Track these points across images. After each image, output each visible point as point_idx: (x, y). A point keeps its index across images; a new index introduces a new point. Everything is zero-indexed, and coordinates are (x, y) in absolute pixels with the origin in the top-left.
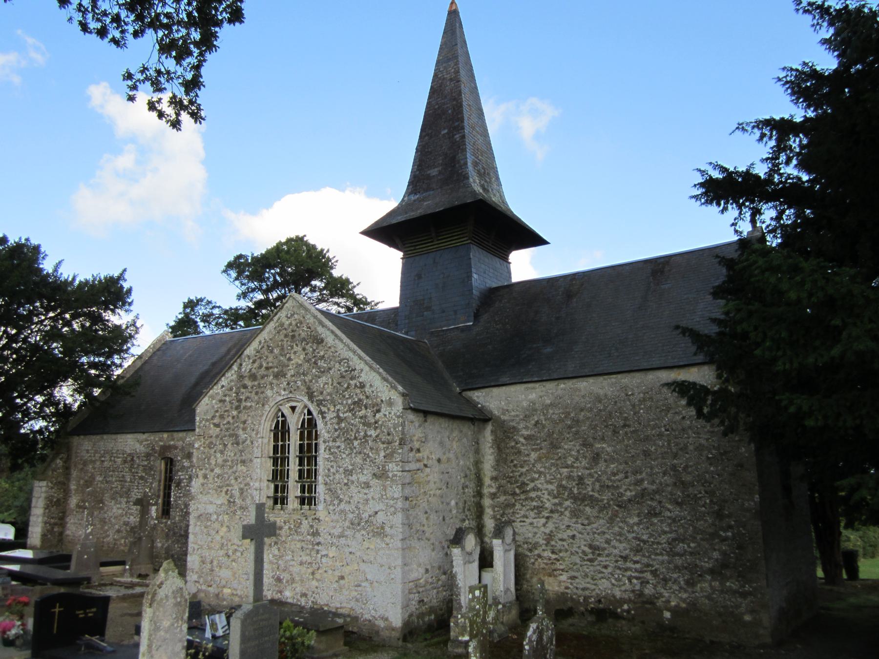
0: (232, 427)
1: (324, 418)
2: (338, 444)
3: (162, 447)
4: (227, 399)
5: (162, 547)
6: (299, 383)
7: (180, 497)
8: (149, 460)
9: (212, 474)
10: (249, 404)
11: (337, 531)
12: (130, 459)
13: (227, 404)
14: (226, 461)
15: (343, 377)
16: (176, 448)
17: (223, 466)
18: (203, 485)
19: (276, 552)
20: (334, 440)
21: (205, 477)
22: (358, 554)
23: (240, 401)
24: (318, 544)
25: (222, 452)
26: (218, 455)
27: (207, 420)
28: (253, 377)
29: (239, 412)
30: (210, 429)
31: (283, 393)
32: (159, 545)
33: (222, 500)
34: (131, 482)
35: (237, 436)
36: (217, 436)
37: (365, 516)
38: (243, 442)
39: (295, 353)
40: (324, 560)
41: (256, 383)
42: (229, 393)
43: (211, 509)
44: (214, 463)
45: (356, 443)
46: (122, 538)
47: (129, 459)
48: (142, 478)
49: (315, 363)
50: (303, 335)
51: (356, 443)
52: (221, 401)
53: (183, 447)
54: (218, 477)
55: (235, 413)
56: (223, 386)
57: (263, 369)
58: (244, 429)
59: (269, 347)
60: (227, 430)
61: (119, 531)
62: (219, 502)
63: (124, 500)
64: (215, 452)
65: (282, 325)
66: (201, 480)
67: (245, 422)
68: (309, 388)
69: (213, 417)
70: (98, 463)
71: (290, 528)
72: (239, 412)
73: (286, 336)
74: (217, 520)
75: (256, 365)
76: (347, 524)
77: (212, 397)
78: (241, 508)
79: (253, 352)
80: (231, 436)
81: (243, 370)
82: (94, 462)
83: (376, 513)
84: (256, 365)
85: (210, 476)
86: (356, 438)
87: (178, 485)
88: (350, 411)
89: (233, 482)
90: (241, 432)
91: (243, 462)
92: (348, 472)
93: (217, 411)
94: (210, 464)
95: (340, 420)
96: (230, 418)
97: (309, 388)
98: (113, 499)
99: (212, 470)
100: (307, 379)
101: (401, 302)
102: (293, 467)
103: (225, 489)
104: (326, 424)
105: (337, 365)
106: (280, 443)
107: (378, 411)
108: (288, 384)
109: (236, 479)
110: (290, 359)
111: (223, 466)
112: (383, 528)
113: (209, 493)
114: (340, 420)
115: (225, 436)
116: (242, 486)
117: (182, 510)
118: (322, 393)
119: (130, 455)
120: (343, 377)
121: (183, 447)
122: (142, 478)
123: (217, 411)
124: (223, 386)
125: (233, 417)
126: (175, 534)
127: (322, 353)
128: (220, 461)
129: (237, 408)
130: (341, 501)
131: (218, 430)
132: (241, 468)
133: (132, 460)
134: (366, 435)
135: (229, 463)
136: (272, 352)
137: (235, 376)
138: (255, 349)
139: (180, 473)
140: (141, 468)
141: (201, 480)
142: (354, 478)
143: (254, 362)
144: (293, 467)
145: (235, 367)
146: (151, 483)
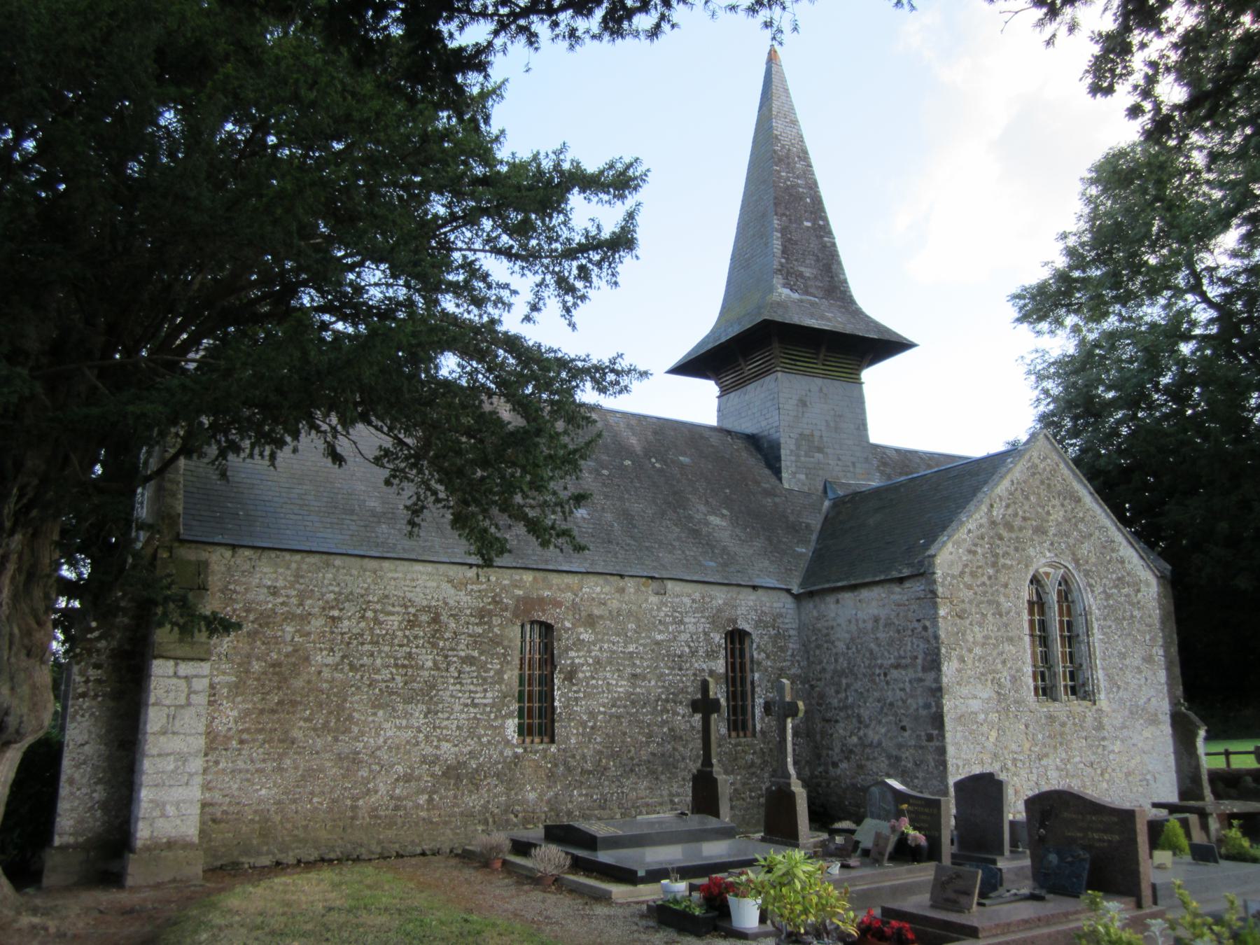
0: (990, 591)
1: (1092, 591)
2: (1109, 623)
3: (518, 599)
4: (979, 550)
5: (540, 797)
6: (1063, 546)
7: (576, 699)
8: (489, 623)
9: (972, 656)
10: (1009, 562)
11: (1117, 723)
12: (432, 621)
13: (979, 557)
14: (986, 637)
15: (1104, 547)
16: (558, 604)
17: (984, 644)
18: (959, 671)
19: (1064, 755)
20: (1105, 619)
21: (962, 660)
22: (1140, 745)
23: (996, 556)
24: (1104, 739)
25: (980, 625)
26: (976, 629)
27: (953, 577)
28: (1009, 527)
29: (997, 571)
30: (960, 590)
31: (1048, 554)
32: (532, 796)
33: (987, 692)
34: (436, 667)
35: (998, 604)
36: (970, 602)
37: (1141, 702)
38: (1008, 613)
39: (1053, 507)
40: (1111, 756)
41: (1013, 536)
42: (981, 542)
43: (975, 705)
44: (971, 640)
45: (1125, 623)
46: (421, 791)
47: (424, 618)
48: (469, 660)
49: (1076, 525)
50: (1059, 487)
51: (1125, 623)
52: (970, 552)
53: (574, 604)
54: (979, 660)
55: (991, 571)
56: (969, 531)
57: (1019, 518)
58: (1006, 596)
59: (1023, 491)
60: (985, 593)
61: (407, 778)
62: (985, 695)
63: (418, 710)
64: (971, 624)
65: (1035, 466)
66: (955, 664)
67: (1006, 586)
68: (1074, 554)
69: (962, 573)
70: (317, 623)
71: (1075, 724)
72: (997, 571)
73: (1042, 482)
74: (985, 720)
75: (1010, 511)
76: (1127, 713)
77: (958, 544)
78: (1016, 702)
79: (1005, 494)
80: (989, 602)
81: (995, 513)
82: (305, 618)
83: (1149, 700)
84: (1010, 511)
85: (969, 658)
86: (1124, 618)
87: (570, 676)
88: (1116, 587)
89: (1000, 666)
90: (1002, 599)
91: (1010, 640)
92: (1123, 656)
93: (966, 566)
94: (966, 641)
95: (1108, 597)
96: (985, 579)
97: (1074, 554)
98: (376, 706)
99: (970, 651)
100: (1071, 541)
101: (876, 446)
102: (1058, 648)
103: (990, 677)
104: (1095, 598)
105: (1097, 533)
106: (1065, 619)
107: (1139, 591)
108: (1052, 544)
109: (1004, 662)
110: (1048, 513)
111: (984, 644)
112: (1156, 715)
113: (969, 682)
114: (1108, 597)
115: (982, 602)
116: (1013, 672)
117: (584, 725)
118: (1087, 562)
119: (427, 609)
120: (1104, 547)
121: (574, 604)
122: (469, 660)
123: (966, 566)
124: (969, 531)
125: (990, 578)
126: (569, 769)
127: (1081, 515)
128: (979, 637)
129: (994, 565)
130: (1119, 688)
131: (971, 592)
132: (1008, 647)
133: (436, 620)
134: (1132, 616)
135: (993, 641)
136: (1027, 498)
137: (984, 521)
138: (1007, 489)
139: (572, 654)
140: (464, 640)
141: (955, 664)
142: (1127, 662)
143: (1008, 506)
144: (1058, 648)
145: (984, 508)
146: (500, 673)
